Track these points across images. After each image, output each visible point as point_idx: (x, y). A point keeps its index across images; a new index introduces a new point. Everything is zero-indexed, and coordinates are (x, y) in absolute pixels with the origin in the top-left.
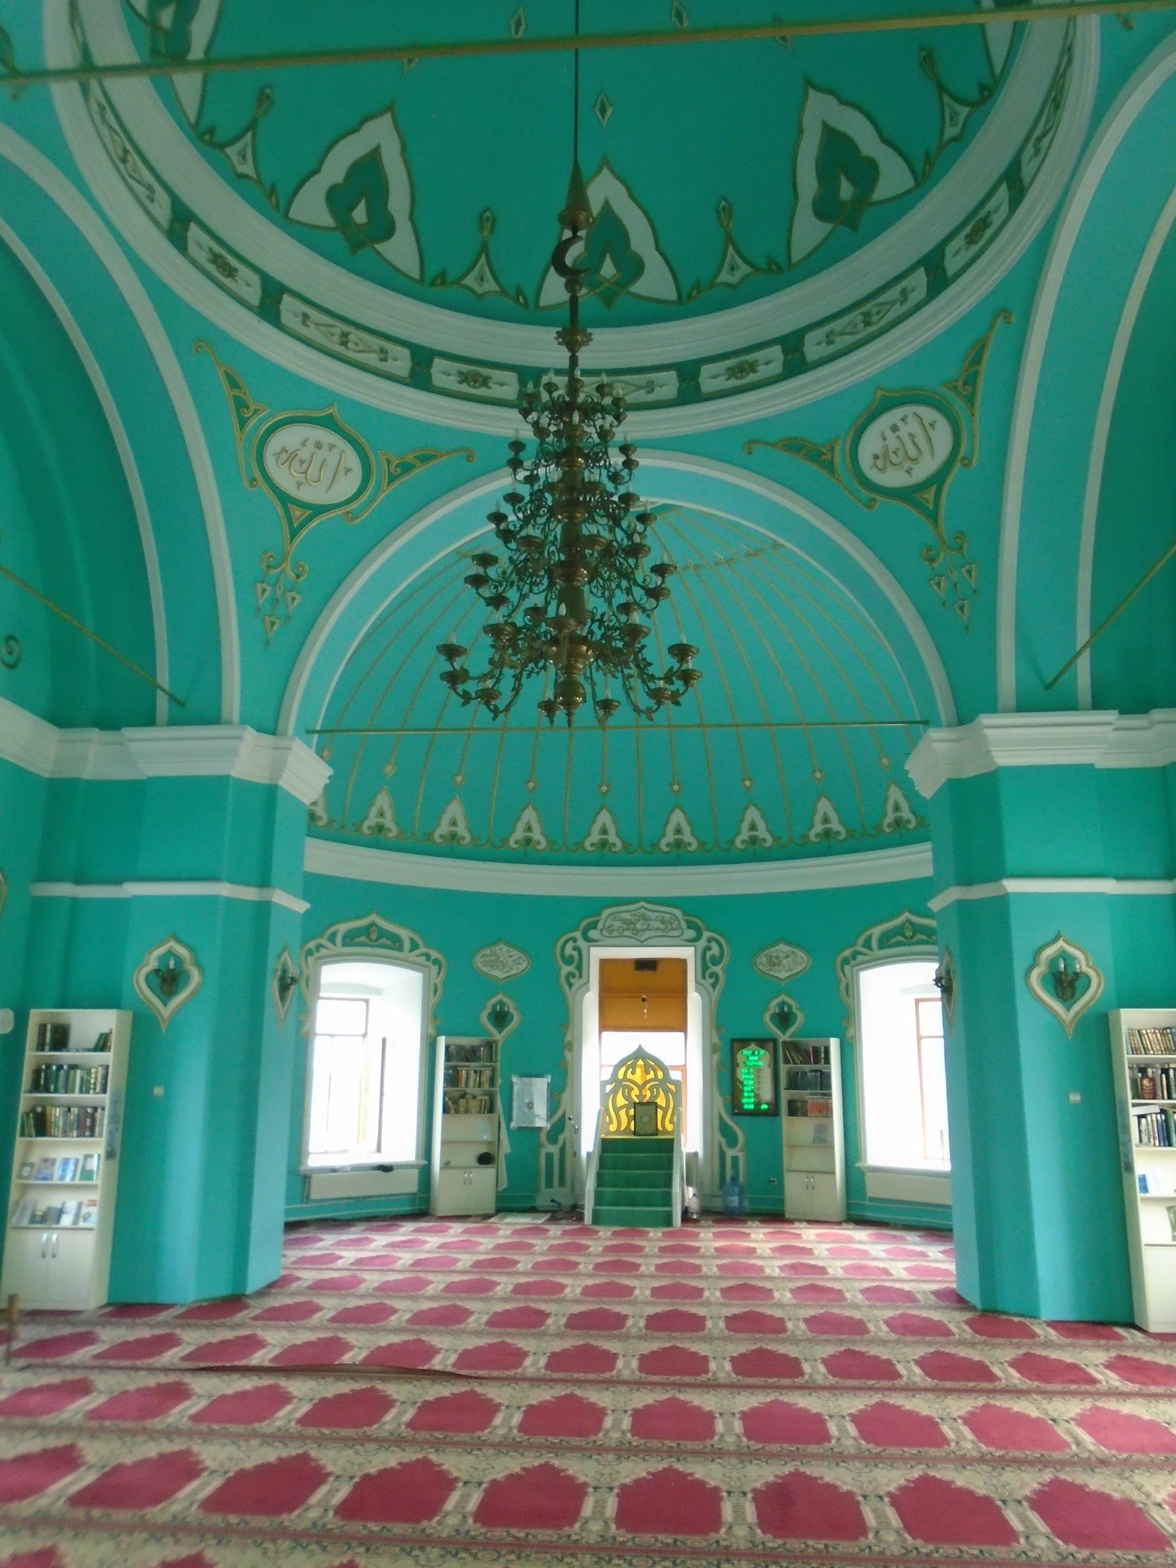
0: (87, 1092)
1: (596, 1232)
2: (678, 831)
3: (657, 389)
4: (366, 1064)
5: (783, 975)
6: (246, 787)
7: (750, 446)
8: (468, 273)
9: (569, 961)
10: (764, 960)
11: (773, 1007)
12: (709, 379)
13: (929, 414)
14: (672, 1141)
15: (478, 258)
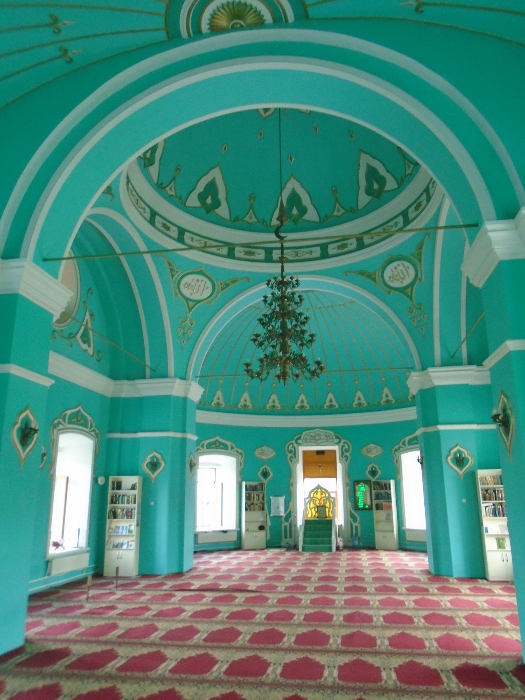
0: (129, 503)
1: (303, 554)
2: (331, 401)
3: (313, 254)
4: (216, 491)
5: (372, 456)
6: (177, 398)
7: (346, 273)
8: (246, 216)
9: (291, 452)
10: (365, 450)
11: (369, 468)
12: (332, 249)
13: (407, 264)
14: (332, 520)
15: (249, 211)
